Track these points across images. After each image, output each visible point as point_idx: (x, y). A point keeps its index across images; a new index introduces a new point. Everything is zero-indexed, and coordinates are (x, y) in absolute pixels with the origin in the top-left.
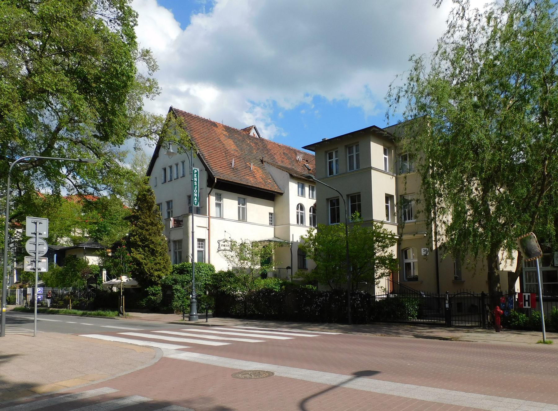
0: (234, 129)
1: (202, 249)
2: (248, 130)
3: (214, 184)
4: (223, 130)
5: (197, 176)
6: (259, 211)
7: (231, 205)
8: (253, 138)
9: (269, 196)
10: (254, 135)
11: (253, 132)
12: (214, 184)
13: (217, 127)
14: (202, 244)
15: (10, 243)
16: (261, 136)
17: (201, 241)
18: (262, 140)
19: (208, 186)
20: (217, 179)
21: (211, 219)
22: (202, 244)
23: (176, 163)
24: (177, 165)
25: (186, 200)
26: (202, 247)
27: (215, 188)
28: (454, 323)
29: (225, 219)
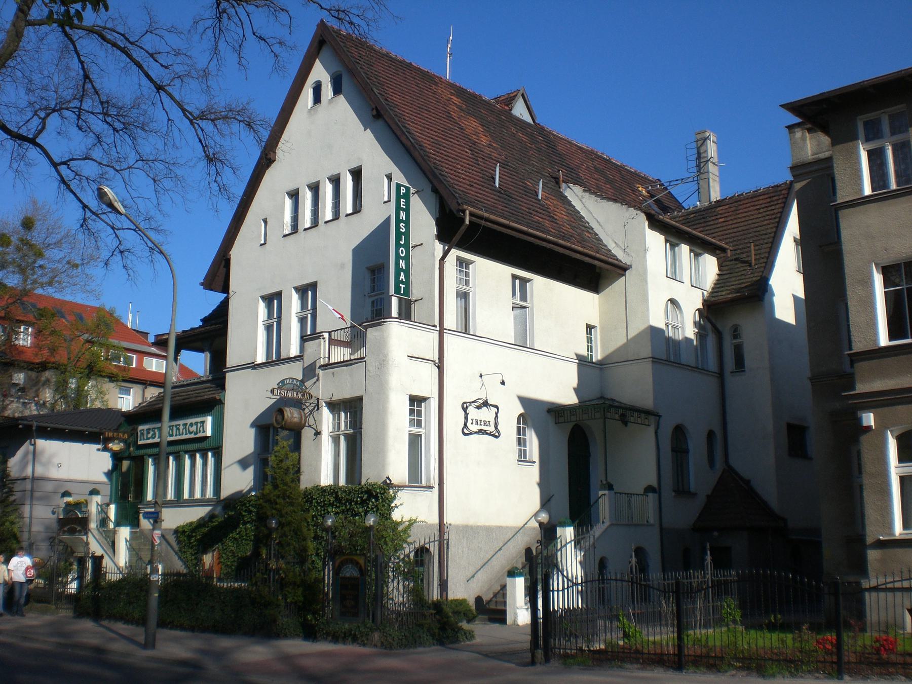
3: (463, 229)
4: (452, 94)
12: (463, 229)
13: (436, 84)
17: (416, 401)
20: (471, 214)
23: (354, 165)
27: (461, 246)
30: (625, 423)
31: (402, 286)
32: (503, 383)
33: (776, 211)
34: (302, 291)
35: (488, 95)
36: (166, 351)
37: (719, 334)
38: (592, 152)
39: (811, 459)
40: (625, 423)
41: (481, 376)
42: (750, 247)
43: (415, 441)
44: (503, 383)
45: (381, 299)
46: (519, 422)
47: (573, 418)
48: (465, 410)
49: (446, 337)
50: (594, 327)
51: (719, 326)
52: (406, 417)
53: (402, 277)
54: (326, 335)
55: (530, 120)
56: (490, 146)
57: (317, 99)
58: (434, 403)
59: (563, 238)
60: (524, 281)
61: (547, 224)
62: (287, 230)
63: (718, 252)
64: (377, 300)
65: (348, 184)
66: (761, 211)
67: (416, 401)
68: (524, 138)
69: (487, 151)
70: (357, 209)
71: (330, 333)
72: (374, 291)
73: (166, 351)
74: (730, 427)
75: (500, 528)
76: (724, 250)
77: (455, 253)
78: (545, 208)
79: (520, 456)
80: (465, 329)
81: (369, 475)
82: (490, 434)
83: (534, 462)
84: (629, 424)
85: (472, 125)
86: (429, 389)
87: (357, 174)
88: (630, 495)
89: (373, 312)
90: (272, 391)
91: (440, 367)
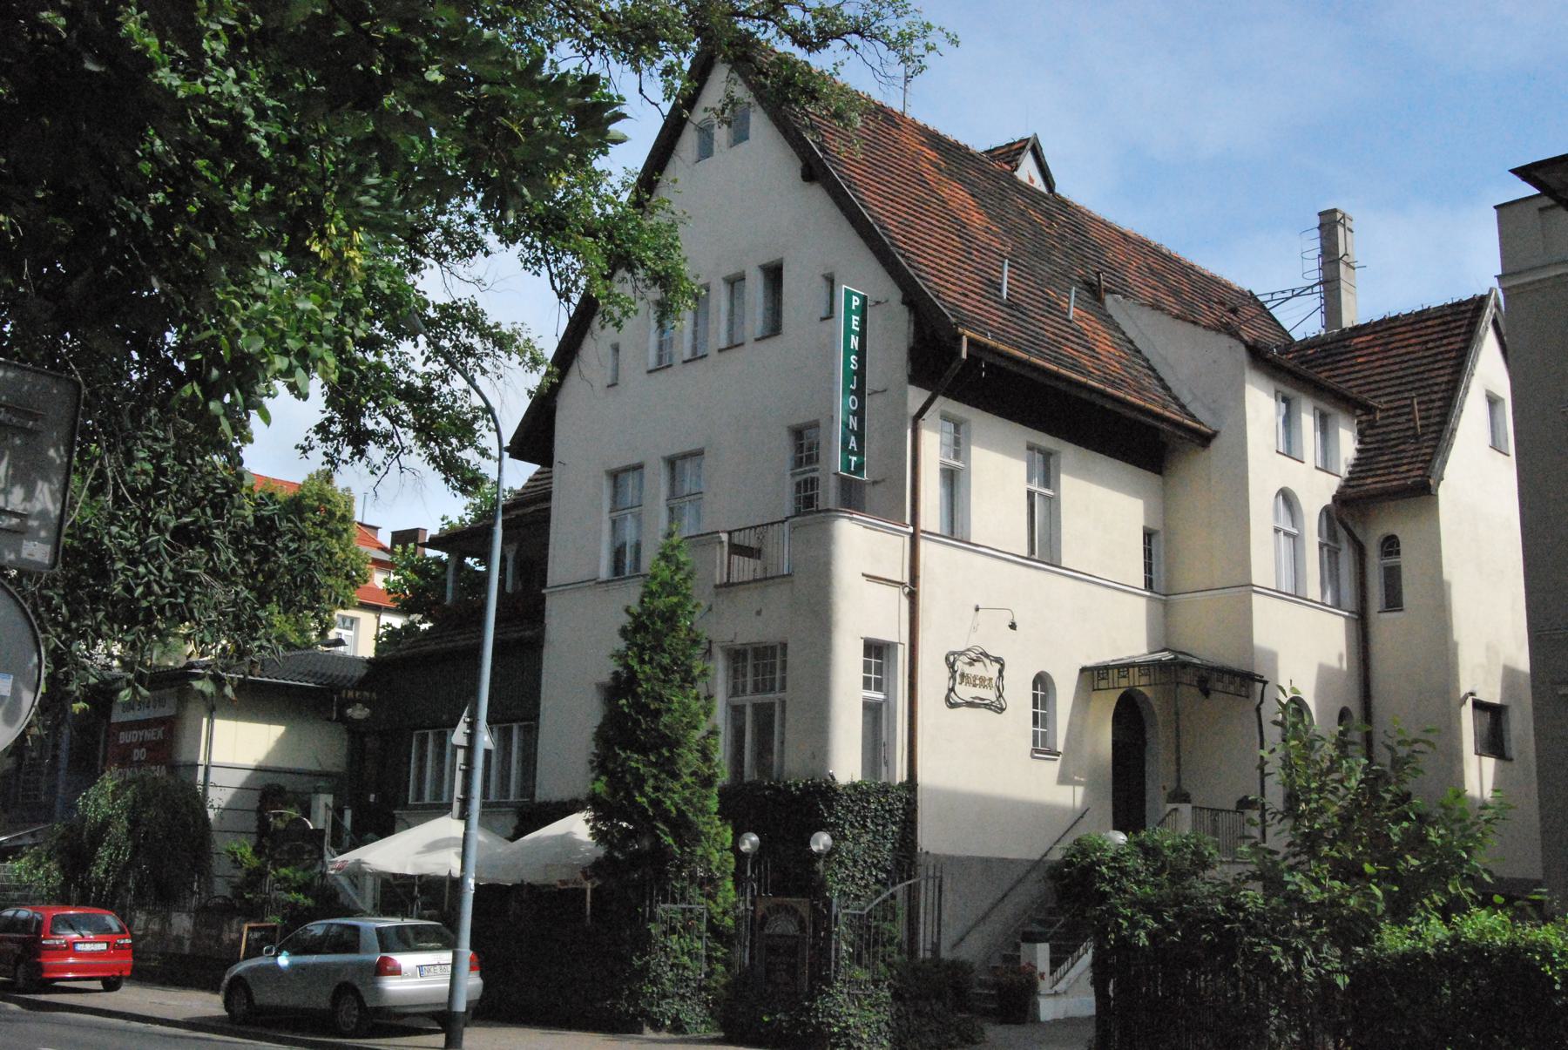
0: (956, 147)
1: (879, 696)
2: (1011, 154)
3: (956, 367)
4: (922, 144)
5: (847, 341)
6: (1105, 510)
7: (999, 470)
8: (1026, 191)
9: (1146, 439)
10: (1032, 181)
11: (1027, 170)
12: (956, 367)
13: (897, 126)
14: (879, 670)
15: (86, 187)
16: (1057, 191)
17: (876, 650)
18: (1064, 204)
19: (916, 378)
20: (971, 342)
21: (734, 579)
22: (879, 670)
23: (767, 258)
24: (735, 282)
25: (784, 450)
26: (879, 688)
27: (949, 394)
28: (445, 800)
29: (974, 548)
30: (1206, 693)
31: (854, 459)
32: (1013, 626)
33: (1456, 346)
34: (671, 462)
35: (979, 143)
36: (772, 705)
37: (1360, 551)
38: (1143, 243)
39: (1511, 760)
40: (1206, 693)
41: (977, 609)
42: (1411, 405)
43: (873, 712)
44: (1013, 626)
45: (813, 479)
46: (1035, 688)
47: (1124, 683)
48: (951, 666)
49: (924, 547)
50: (1156, 532)
51: (1358, 532)
52: (859, 674)
53: (853, 444)
54: (725, 537)
55: (1043, 189)
56: (987, 230)
57: (706, 151)
58: (902, 655)
59: (1113, 384)
60: (1047, 455)
61: (1085, 361)
62: (652, 362)
63: (1359, 412)
64: (806, 481)
65: (755, 287)
66: (1431, 345)
67: (876, 650)
68: (1038, 218)
69: (983, 237)
70: (774, 327)
71: (730, 533)
72: (800, 466)
73: (772, 705)
74: (1375, 702)
75: (1004, 861)
76: (1369, 410)
77: (942, 403)
78: (1080, 334)
79: (1035, 742)
80: (955, 530)
81: (792, 765)
82: (988, 706)
83: (1058, 754)
84: (1213, 695)
85: (957, 196)
86: (893, 630)
87: (774, 274)
88: (1216, 812)
89: (798, 500)
90: (348, 489)
91: (913, 597)
